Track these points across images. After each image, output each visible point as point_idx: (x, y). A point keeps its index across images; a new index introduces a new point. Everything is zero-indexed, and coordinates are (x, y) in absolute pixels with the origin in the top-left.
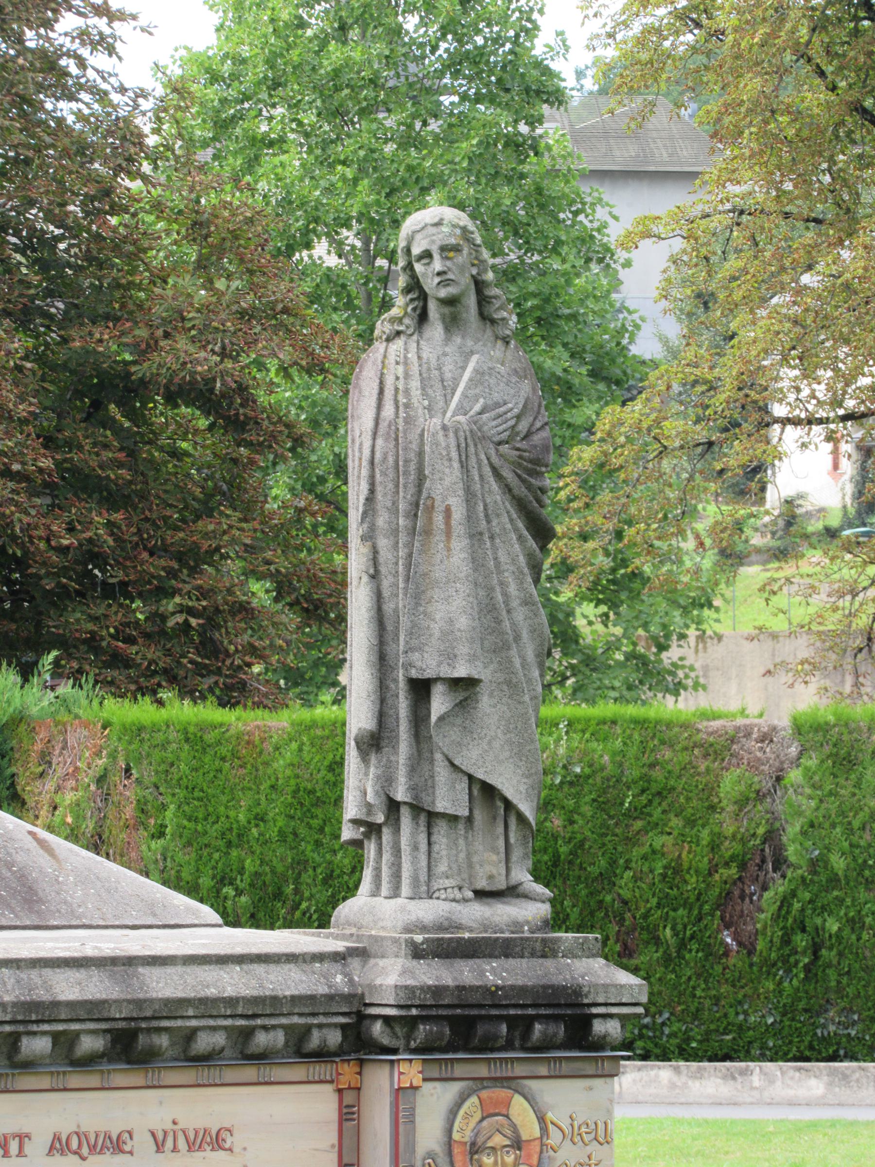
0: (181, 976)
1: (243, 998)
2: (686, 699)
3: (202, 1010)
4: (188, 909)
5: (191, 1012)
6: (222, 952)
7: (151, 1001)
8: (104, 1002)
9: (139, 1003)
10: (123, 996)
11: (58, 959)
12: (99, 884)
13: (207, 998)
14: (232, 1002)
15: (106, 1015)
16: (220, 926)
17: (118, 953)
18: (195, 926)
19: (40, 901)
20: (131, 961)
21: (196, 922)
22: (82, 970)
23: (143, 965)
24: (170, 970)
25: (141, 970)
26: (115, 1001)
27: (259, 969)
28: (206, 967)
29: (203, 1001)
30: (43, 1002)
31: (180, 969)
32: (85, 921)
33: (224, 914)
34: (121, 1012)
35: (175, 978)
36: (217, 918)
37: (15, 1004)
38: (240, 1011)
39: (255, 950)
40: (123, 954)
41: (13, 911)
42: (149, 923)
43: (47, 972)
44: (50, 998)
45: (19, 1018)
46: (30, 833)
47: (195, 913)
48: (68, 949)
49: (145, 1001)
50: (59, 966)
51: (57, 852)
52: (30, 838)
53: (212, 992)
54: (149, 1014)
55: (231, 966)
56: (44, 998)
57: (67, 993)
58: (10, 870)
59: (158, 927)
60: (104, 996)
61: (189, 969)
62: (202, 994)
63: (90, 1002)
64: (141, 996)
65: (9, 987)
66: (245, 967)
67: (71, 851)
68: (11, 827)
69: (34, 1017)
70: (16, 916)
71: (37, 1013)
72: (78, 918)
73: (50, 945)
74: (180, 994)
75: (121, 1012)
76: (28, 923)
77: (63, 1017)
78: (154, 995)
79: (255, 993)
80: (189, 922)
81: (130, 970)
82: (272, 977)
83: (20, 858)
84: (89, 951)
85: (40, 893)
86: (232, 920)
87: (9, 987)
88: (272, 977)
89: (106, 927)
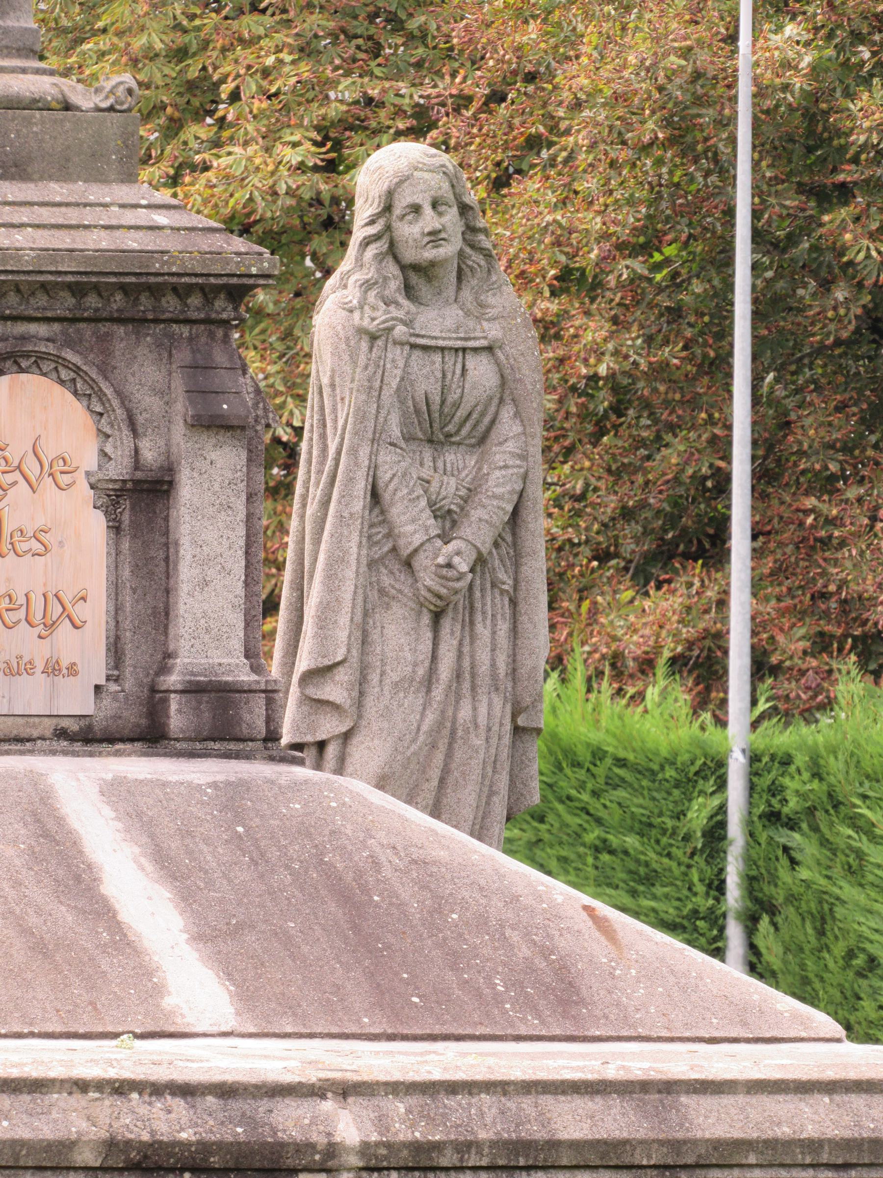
0: (742, 1110)
1: (829, 1141)
2: (664, 693)
3: (768, 1157)
4: (795, 1016)
5: (752, 1159)
6: (805, 1077)
7: (695, 1142)
8: (625, 1142)
9: (676, 1145)
10: (652, 1135)
11: (563, 1082)
12: (672, 979)
13: (776, 1141)
14: (813, 1145)
15: (627, 1161)
16: (838, 1040)
17: (653, 1075)
18: (802, 1040)
19: (582, 1002)
20: (670, 1087)
21: (804, 1034)
22: (598, 1099)
23: (687, 1092)
24: (727, 1100)
25: (683, 1099)
26: (642, 1142)
27: (858, 1101)
28: (780, 1098)
29: (771, 1144)
30: (536, 1142)
31: (741, 1099)
32: (641, 1031)
33: (848, 1027)
34: (649, 1157)
35: (733, 1111)
36: (838, 1030)
37: (493, 1144)
38: (825, 1158)
39: (853, 1075)
40: (659, 1077)
41: (539, 1016)
42: (734, 1035)
43: (547, 1100)
44: (547, 1137)
45: (501, 1162)
46: (586, 908)
47: (805, 1022)
48: (580, 1069)
49: (685, 1142)
50: (564, 1093)
51: (620, 934)
52: (584, 915)
53: (785, 1131)
54: (690, 1160)
55: (817, 1096)
56: (537, 1136)
57: (571, 1130)
58: (546, 958)
59: (748, 1041)
60: (625, 1135)
61: (754, 1100)
62: (770, 1134)
63: (605, 1142)
64: (680, 1135)
65: (488, 1120)
66: (837, 1098)
67: (640, 933)
68: (560, 899)
69: (522, 1162)
70: (543, 1022)
71: (527, 1156)
72: (633, 1026)
73: (491, 1061)
74: (737, 1134)
75: (649, 1157)
76: (558, 1032)
77: (565, 1162)
78: (699, 1135)
79: (848, 1134)
80: (792, 1034)
81: (668, 1100)
82: (875, 1113)
83: (563, 943)
84: (611, 1073)
85: (584, 992)
86: (857, 1031)
87: (488, 1120)
88: (875, 1113)
89: (672, 1040)
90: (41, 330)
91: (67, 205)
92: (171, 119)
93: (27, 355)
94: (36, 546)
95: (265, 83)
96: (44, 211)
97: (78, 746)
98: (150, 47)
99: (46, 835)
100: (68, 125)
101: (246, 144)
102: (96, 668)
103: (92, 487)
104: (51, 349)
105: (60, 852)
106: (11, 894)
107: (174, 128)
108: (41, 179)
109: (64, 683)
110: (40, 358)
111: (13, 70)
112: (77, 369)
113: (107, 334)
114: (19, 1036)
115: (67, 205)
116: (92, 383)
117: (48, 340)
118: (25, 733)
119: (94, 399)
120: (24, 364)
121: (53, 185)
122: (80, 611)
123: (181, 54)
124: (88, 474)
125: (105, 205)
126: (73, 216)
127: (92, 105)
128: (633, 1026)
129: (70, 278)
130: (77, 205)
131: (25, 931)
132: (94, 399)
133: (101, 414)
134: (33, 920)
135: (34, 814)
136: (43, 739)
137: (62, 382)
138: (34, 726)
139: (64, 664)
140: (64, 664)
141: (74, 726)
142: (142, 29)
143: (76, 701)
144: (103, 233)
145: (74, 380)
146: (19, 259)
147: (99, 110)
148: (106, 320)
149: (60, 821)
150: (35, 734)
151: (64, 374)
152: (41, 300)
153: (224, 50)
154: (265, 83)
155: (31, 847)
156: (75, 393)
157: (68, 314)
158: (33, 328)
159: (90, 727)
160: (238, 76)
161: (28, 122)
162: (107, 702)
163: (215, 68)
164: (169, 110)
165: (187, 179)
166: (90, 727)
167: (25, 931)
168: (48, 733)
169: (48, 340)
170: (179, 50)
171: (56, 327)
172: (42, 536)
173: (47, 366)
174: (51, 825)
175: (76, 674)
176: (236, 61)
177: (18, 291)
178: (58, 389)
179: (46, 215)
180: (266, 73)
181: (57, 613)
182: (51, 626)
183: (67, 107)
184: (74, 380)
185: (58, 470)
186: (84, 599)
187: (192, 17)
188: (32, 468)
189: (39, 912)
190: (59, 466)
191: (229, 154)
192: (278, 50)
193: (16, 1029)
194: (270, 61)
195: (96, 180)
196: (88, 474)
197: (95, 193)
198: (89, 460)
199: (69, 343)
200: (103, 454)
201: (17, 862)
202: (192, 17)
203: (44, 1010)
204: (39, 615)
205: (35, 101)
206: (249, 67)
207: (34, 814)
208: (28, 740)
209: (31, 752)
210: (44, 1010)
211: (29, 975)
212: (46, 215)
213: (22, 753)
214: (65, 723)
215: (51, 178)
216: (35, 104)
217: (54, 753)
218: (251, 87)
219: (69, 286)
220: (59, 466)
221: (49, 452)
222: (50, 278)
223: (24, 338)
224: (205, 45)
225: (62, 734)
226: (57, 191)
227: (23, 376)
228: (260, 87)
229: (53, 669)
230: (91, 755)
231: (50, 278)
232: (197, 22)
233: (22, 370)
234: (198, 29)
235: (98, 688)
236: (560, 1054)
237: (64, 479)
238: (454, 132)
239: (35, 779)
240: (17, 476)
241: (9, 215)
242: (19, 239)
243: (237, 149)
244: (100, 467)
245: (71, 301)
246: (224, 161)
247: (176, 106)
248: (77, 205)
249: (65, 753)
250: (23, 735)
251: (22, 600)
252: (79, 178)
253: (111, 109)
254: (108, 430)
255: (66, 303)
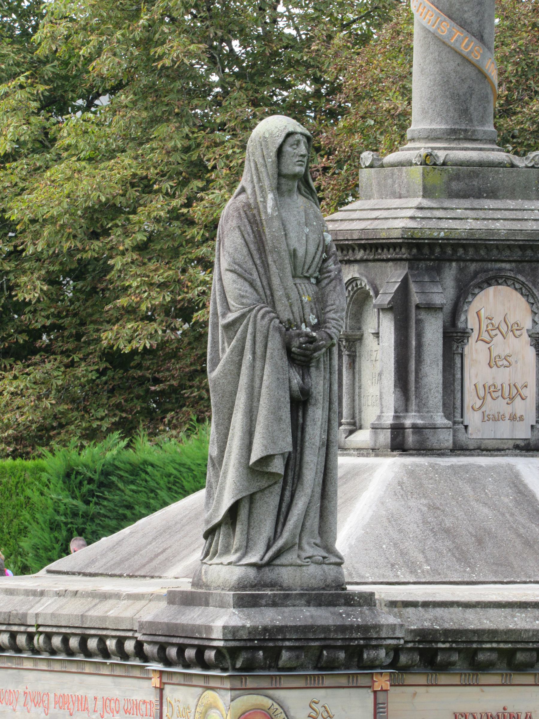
90: (507, 266)
91: (516, 210)
92: (184, 178)
93: (501, 277)
94: (506, 363)
95: (227, 162)
96: (506, 212)
97: (524, 452)
98: (176, 146)
99: (520, 492)
100: (514, 174)
101: (220, 189)
102: (531, 418)
103: (530, 336)
104: (512, 274)
105: (528, 500)
106: (511, 519)
107: (184, 183)
108: (503, 198)
109: (517, 424)
110: (508, 278)
111: (489, 150)
112: (523, 284)
113: (535, 268)
114: (525, 583)
115: (516, 210)
116: (529, 290)
117: (510, 270)
118: (502, 446)
119: (530, 297)
120: (500, 281)
121: (508, 201)
122: (525, 392)
123: (187, 150)
124: (528, 330)
125: (532, 210)
126: (519, 215)
127: (524, 165)
128: (363, 577)
129: (521, 243)
130: (520, 210)
131: (519, 536)
132: (530, 297)
133: (533, 304)
134: (522, 531)
135: (513, 483)
136: (509, 449)
137: (516, 289)
138: (505, 444)
139: (518, 415)
140: (518, 415)
141: (522, 444)
142: (171, 138)
143: (523, 432)
144: (534, 222)
145: (521, 289)
146: (499, 234)
147: (527, 167)
148: (535, 261)
149: (525, 486)
150: (506, 447)
151: (517, 286)
152: (507, 253)
153: (208, 147)
154: (227, 162)
155: (515, 498)
156: (522, 294)
157: (519, 259)
158: (503, 265)
159: (529, 444)
160: (215, 159)
161: (497, 173)
162: (536, 432)
163: (204, 156)
164: (184, 174)
165: (195, 205)
166: (529, 444)
167: (519, 536)
168: (511, 447)
169: (510, 270)
170: (187, 148)
171: (513, 264)
172: (508, 358)
173: (510, 282)
174: (521, 488)
175: (523, 420)
176: (214, 153)
177: (486, 248)
178: (515, 293)
179: (508, 215)
180: (227, 157)
181: (513, 394)
182: (512, 399)
183: (513, 166)
184: (521, 289)
185: (515, 329)
186: (526, 386)
187: (193, 133)
188: (504, 328)
189: (524, 527)
190: (515, 327)
191: (213, 193)
192: (233, 147)
193: (524, 579)
194: (230, 152)
195: (527, 199)
196: (528, 330)
197: (527, 204)
198: (528, 324)
199: (519, 272)
200: (534, 321)
201: (510, 505)
202: (193, 133)
203: (534, 571)
204: (507, 394)
205: (500, 163)
206: (220, 155)
207: (513, 483)
208: (503, 450)
209: (507, 455)
210: (534, 571)
211: (525, 556)
212: (508, 215)
213: (503, 456)
214: (518, 442)
215: (507, 198)
216: (500, 165)
217: (516, 455)
218: (221, 164)
219: (520, 246)
220: (515, 327)
221: (511, 320)
222: (513, 242)
223: (500, 270)
224: (198, 145)
225: (517, 447)
226: (511, 204)
227: (500, 287)
228: (225, 163)
229: (513, 418)
230: (532, 456)
231: (513, 242)
232: (195, 135)
233: (499, 284)
234: (195, 138)
235: (532, 426)
236: (521, 589)
237: (517, 333)
238: (323, 183)
239: (511, 468)
240: (497, 331)
241: (537, 215)
242: (498, 225)
243: (217, 191)
244: (533, 327)
245: (520, 253)
246: (211, 196)
247: (187, 173)
248: (520, 210)
249: (521, 456)
250: (501, 448)
251: (500, 387)
252: (519, 198)
253: (533, 167)
254: (536, 311)
255: (517, 254)
